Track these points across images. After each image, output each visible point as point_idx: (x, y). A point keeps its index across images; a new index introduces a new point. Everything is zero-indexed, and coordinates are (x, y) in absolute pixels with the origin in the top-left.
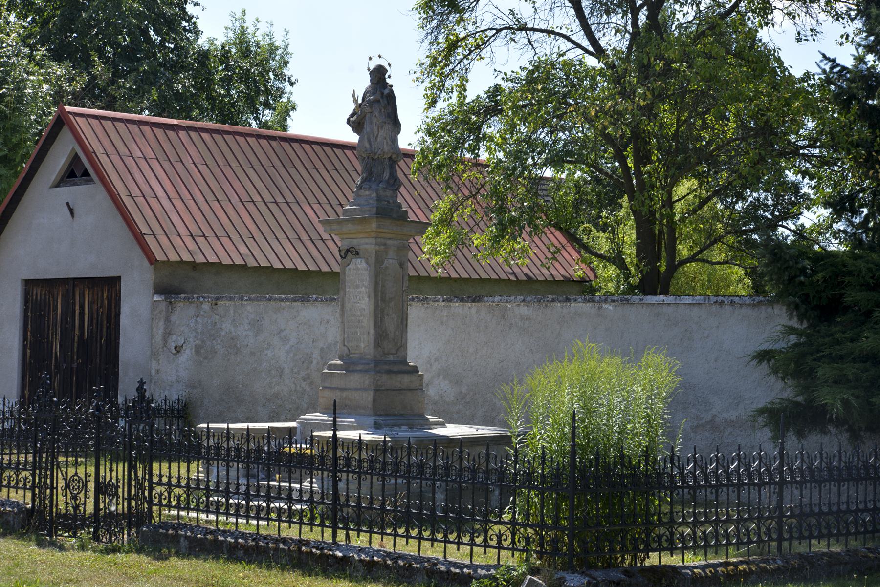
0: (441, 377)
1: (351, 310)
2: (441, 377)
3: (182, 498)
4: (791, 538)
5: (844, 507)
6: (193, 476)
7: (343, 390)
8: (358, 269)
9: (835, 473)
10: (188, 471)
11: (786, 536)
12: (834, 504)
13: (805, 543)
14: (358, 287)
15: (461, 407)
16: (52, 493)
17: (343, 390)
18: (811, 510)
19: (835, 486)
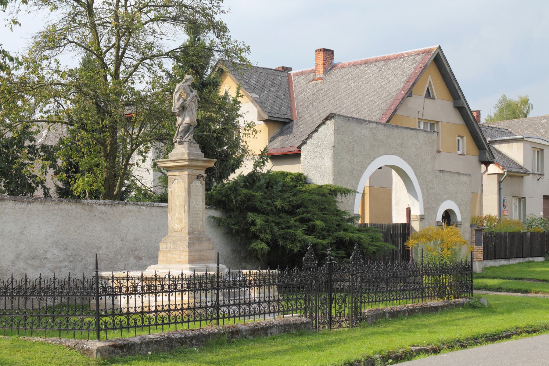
0: (54, 247)
1: (194, 208)
2: (54, 247)
3: (246, 310)
4: (224, 318)
5: (272, 299)
6: (159, 303)
7: (200, 251)
8: (197, 186)
9: (192, 286)
10: (269, 293)
11: (221, 316)
12: (159, 306)
13: (198, 323)
14: (197, 195)
15: (67, 264)
16: (352, 300)
17: (200, 251)
18: (245, 301)
19: (139, 297)
